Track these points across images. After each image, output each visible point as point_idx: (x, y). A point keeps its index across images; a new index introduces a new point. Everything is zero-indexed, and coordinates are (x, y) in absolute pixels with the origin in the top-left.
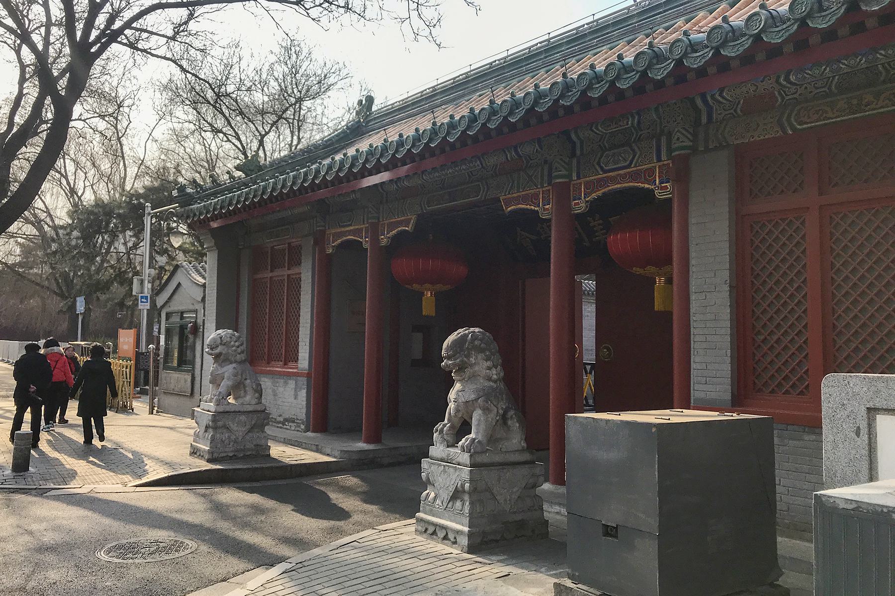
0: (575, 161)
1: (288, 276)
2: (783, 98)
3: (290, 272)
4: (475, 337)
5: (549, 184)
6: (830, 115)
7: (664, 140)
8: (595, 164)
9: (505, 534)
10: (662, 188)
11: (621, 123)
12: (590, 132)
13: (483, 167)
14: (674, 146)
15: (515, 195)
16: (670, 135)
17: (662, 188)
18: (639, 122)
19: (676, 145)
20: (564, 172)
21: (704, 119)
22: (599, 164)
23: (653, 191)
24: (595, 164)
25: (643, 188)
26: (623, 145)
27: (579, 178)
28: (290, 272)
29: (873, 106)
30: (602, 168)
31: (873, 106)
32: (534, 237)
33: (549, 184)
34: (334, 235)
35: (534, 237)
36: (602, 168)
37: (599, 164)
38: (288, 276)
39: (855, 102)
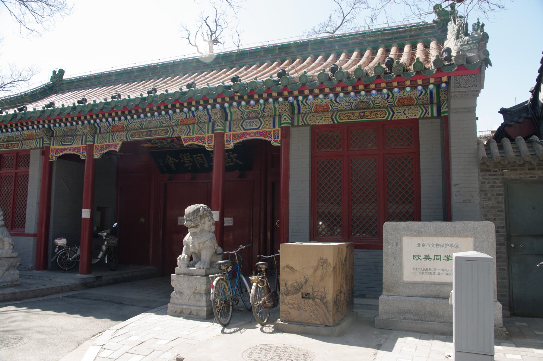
0: (228, 123)
1: (16, 173)
2: (332, 108)
3: (17, 171)
4: (204, 209)
5: (213, 133)
6: (352, 118)
7: (277, 119)
8: (240, 125)
9: (232, 311)
10: (275, 141)
11: (379, 116)
12: (237, 109)
13: (170, 119)
14: (282, 122)
15: (191, 137)
16: (280, 116)
17: (275, 141)
18: (264, 108)
19: (284, 122)
20: (222, 128)
21: (296, 112)
22: (242, 125)
23: (270, 142)
24: (240, 125)
25: (265, 140)
26: (254, 118)
27: (230, 131)
28: (17, 171)
29: (369, 117)
30: (243, 128)
31: (369, 117)
32: (177, 161)
33: (213, 133)
34: (57, 150)
35: (177, 161)
36: (243, 128)
37: (242, 125)
38: (16, 173)
39: (362, 114)
